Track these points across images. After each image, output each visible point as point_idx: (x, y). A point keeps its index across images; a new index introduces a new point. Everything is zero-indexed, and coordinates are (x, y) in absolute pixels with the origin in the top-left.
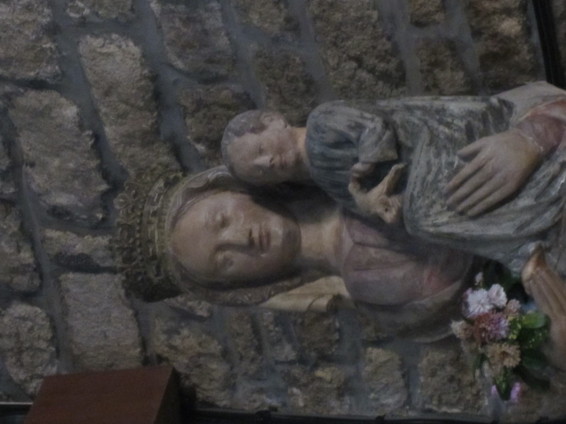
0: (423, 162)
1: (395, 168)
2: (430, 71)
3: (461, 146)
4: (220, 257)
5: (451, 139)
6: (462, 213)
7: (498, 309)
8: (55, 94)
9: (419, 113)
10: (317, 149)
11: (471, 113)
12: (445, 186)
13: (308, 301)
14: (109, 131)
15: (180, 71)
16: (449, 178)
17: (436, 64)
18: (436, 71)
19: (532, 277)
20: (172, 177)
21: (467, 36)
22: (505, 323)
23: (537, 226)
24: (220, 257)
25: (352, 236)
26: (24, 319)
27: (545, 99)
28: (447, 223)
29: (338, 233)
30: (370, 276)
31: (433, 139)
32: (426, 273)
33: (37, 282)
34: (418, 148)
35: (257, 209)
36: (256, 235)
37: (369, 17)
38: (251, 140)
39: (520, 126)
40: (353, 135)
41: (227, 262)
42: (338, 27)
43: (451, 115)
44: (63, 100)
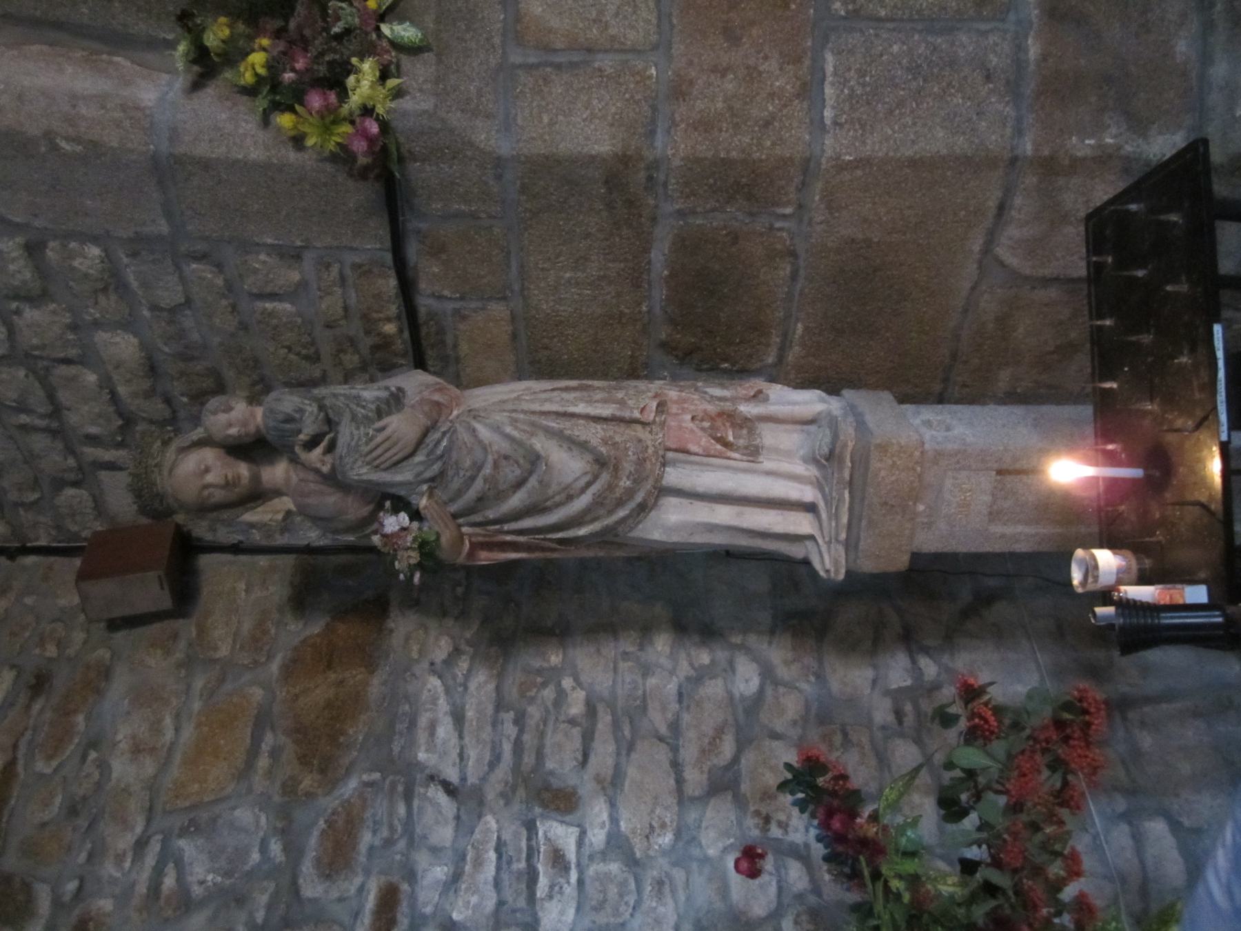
0: (348, 434)
1: (327, 438)
2: (337, 356)
3: (373, 423)
4: (206, 493)
5: (366, 417)
6: (377, 467)
7: (404, 529)
8: (80, 367)
9: (342, 398)
10: (272, 424)
11: (378, 399)
12: (366, 449)
13: (269, 516)
14: (122, 390)
15: (166, 354)
16: (367, 443)
17: (341, 351)
18: (341, 355)
19: (426, 507)
20: (166, 437)
21: (362, 334)
22: (410, 538)
23: (428, 474)
24: (206, 493)
25: (297, 475)
26: (73, 497)
27: (427, 386)
28: (366, 473)
29: (287, 472)
30: (312, 501)
31: (354, 418)
32: (350, 499)
33: (80, 476)
34: (343, 424)
35: (230, 460)
36: (230, 477)
37: (296, 322)
38: (222, 418)
39: (413, 407)
40: (297, 416)
41: (210, 496)
42: (275, 327)
43: (365, 400)
44: (85, 371)
